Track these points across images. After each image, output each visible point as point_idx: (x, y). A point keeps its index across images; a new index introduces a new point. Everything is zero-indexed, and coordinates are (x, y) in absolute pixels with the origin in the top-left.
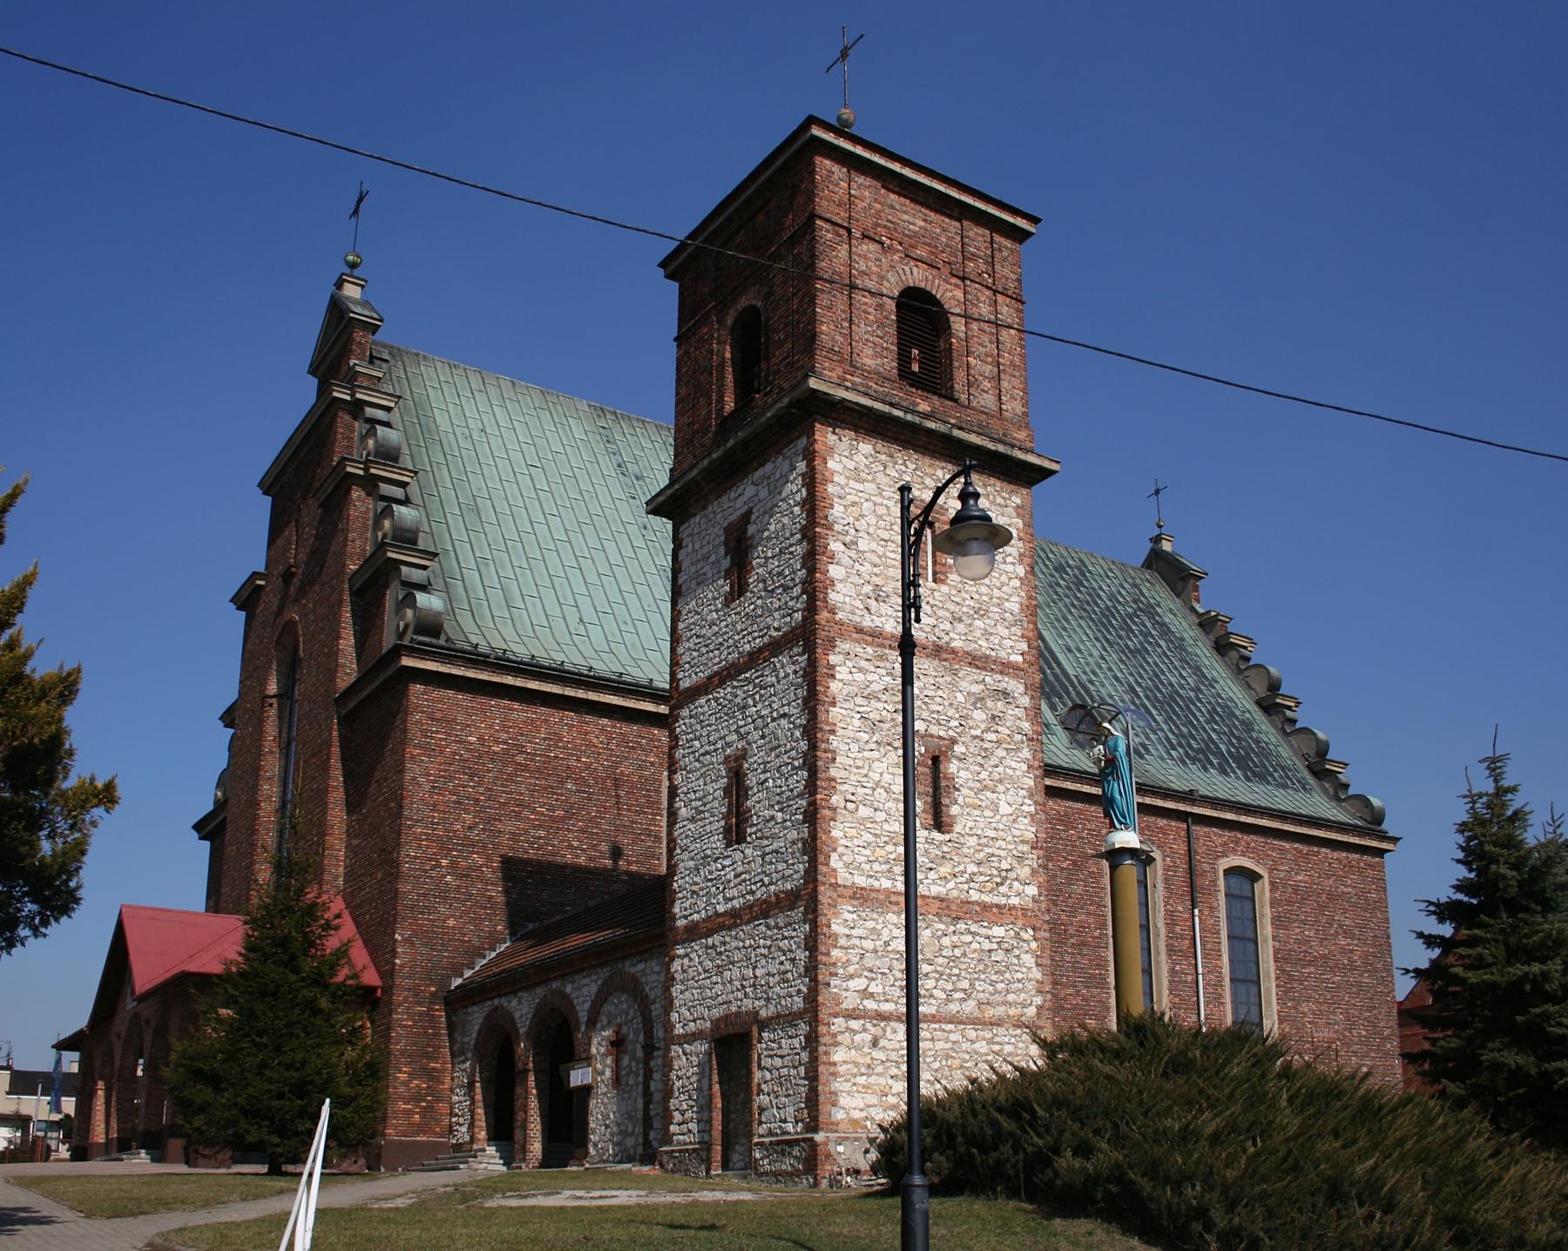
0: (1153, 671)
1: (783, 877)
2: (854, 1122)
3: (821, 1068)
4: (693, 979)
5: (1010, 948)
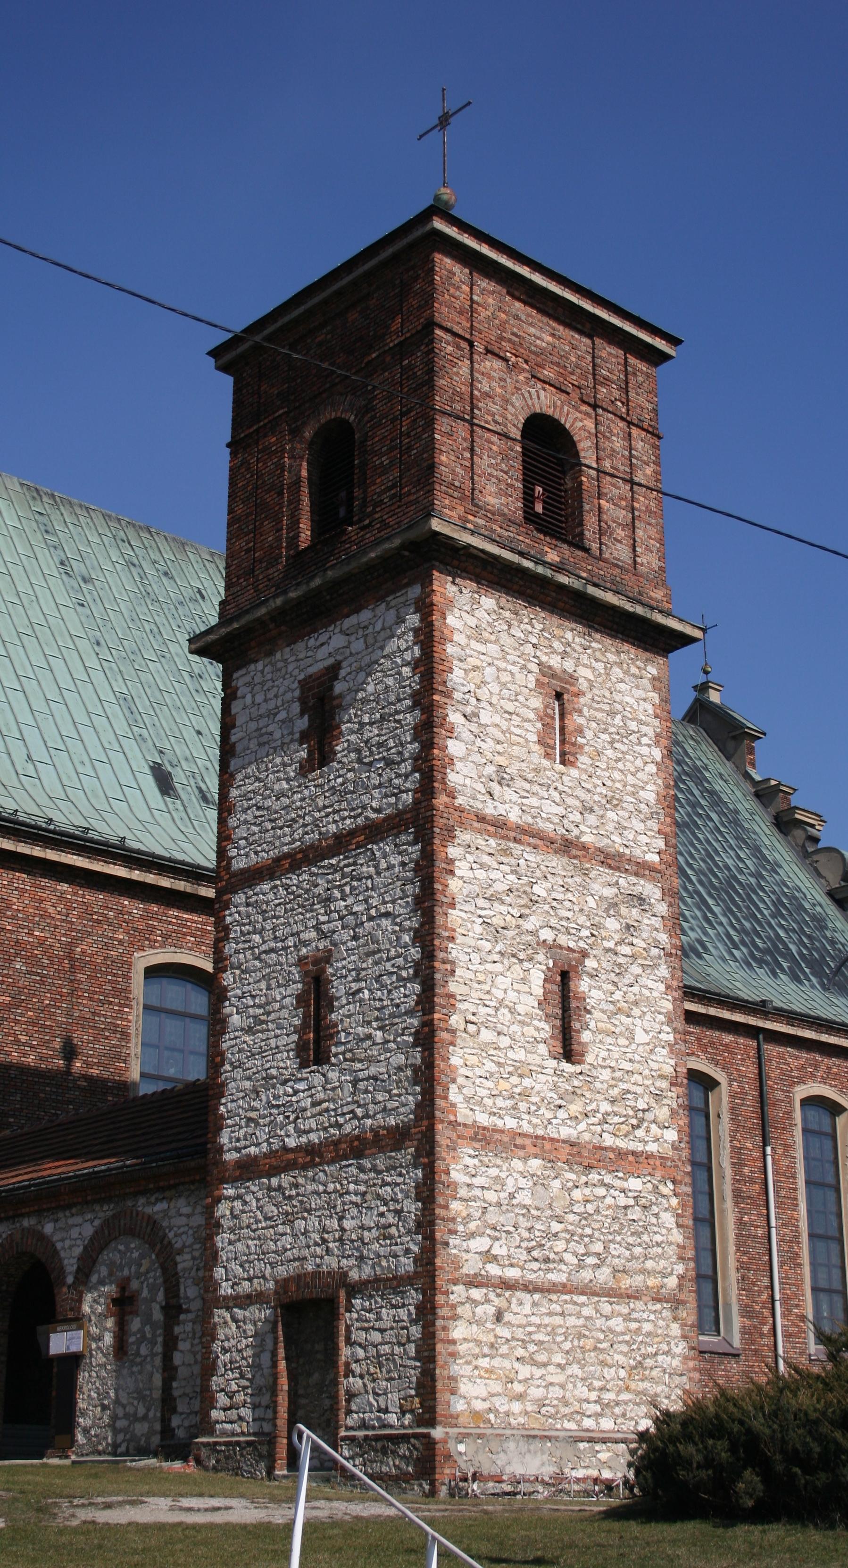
0: (706, 850)
1: (384, 1109)
2: (476, 1415)
3: (439, 1347)
4: (248, 1227)
5: (648, 1204)
